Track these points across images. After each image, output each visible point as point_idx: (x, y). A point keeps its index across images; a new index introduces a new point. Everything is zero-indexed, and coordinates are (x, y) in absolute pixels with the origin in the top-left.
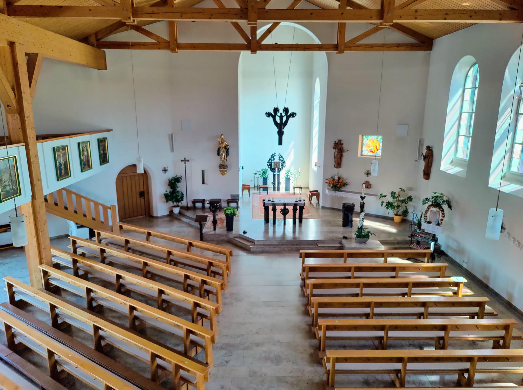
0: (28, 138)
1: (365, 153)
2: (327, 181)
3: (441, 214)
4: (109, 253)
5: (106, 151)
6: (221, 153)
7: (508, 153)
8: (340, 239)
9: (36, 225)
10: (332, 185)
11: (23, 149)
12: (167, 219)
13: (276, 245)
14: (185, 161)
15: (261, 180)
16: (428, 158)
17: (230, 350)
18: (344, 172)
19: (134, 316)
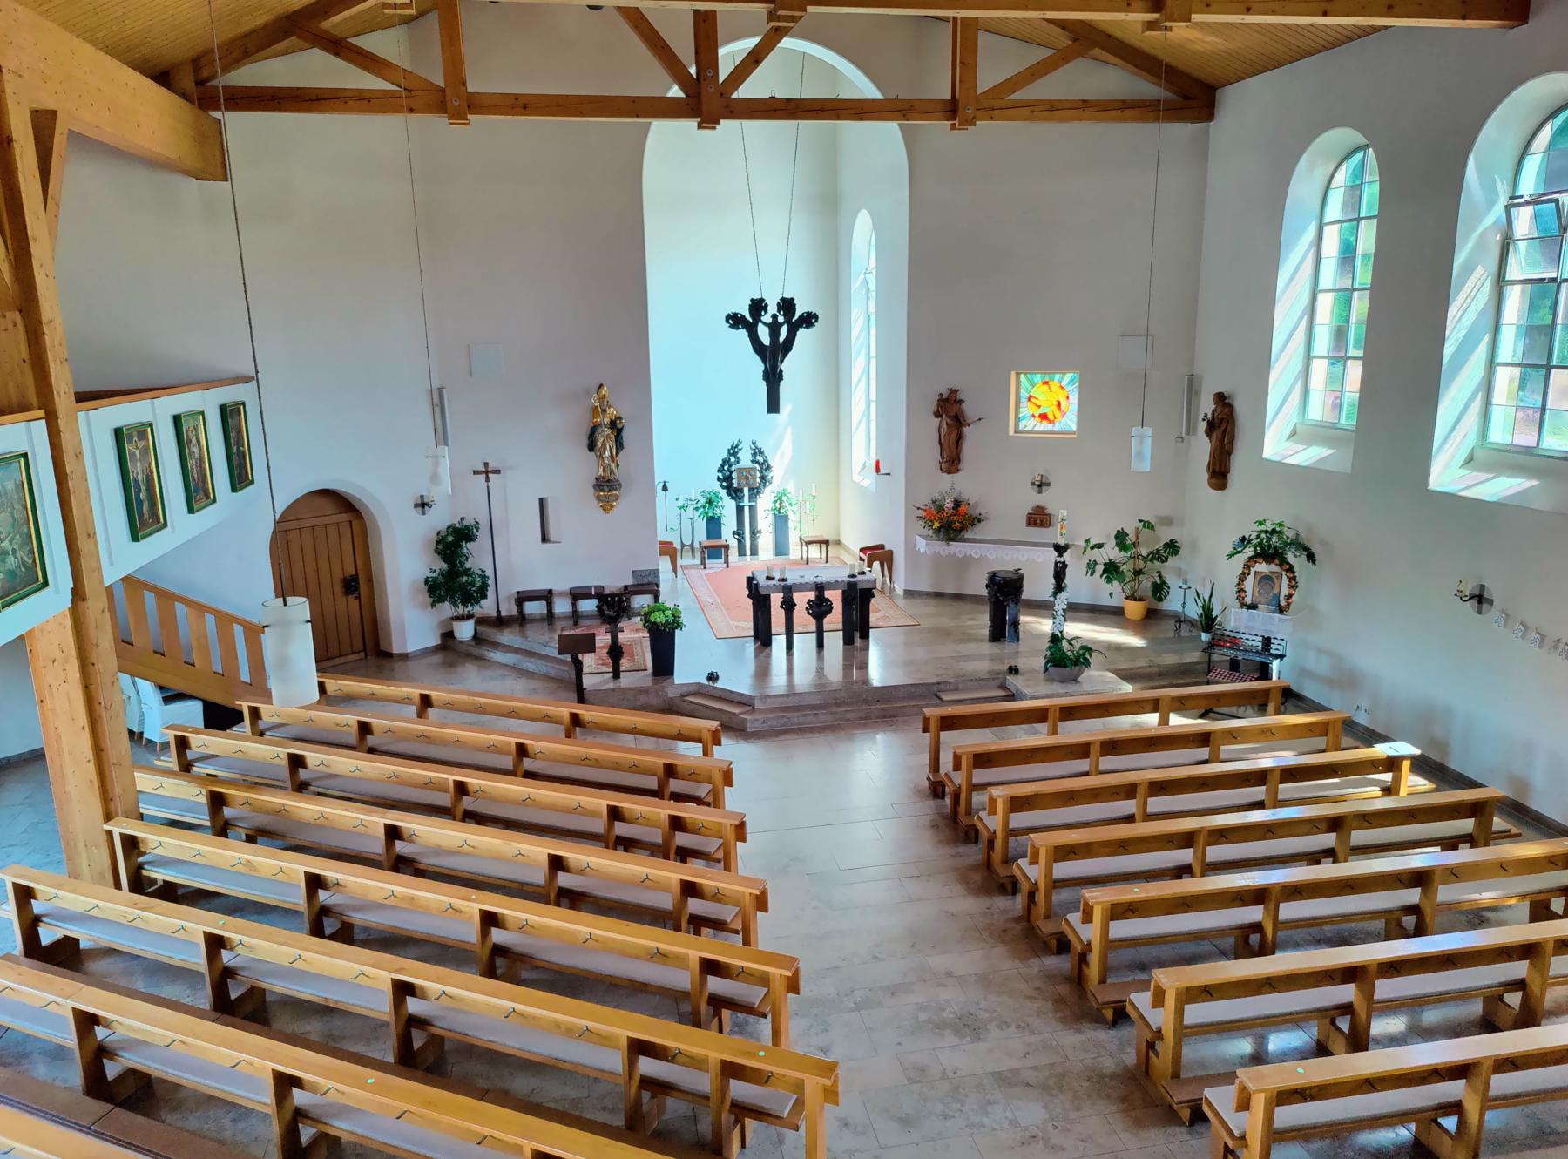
0: (55, 393)
1: (1026, 426)
2: (923, 514)
3: (1285, 581)
4: (322, 768)
5: (243, 446)
6: (599, 444)
7: (1480, 394)
8: (1000, 676)
9: (87, 687)
10: (937, 525)
11: (40, 427)
12: (437, 658)
13: (821, 707)
14: (487, 472)
15: (701, 526)
16: (1223, 428)
17: (816, 1015)
18: (967, 485)
19: (491, 947)
